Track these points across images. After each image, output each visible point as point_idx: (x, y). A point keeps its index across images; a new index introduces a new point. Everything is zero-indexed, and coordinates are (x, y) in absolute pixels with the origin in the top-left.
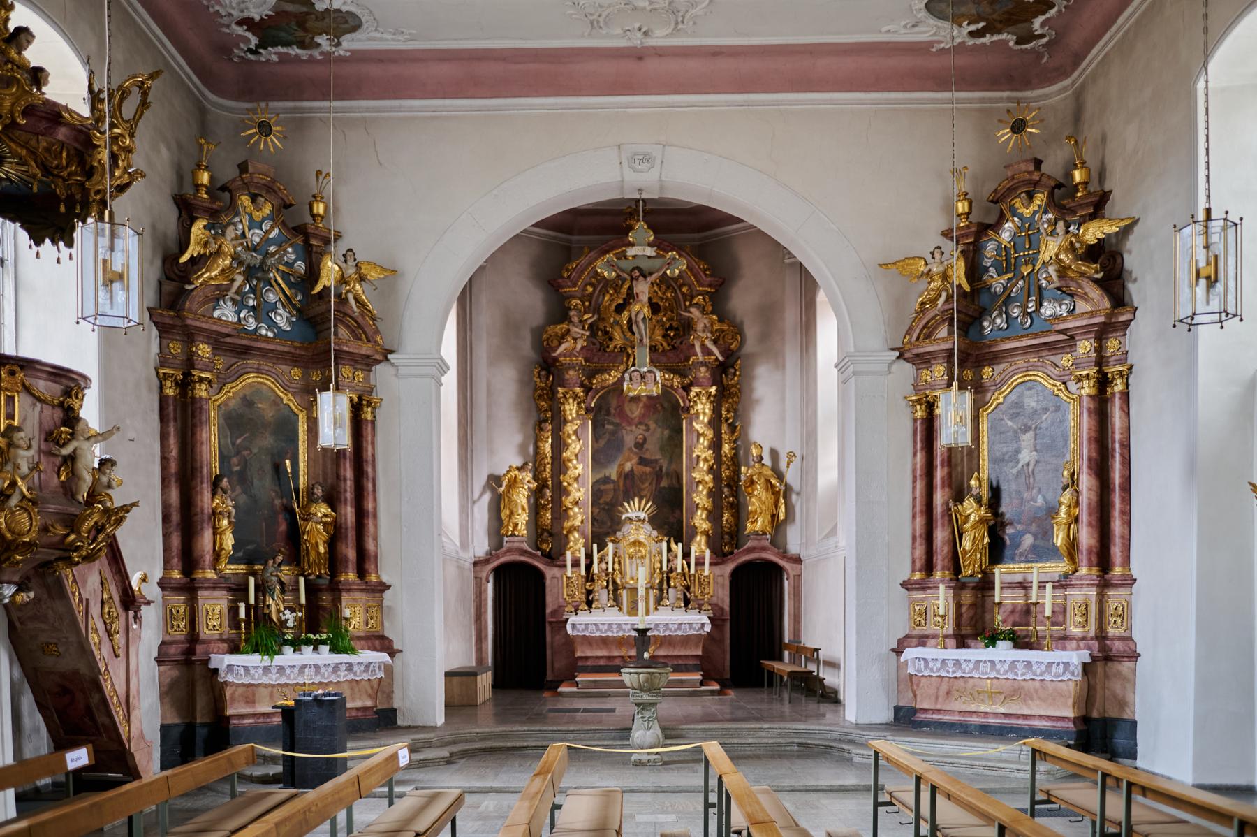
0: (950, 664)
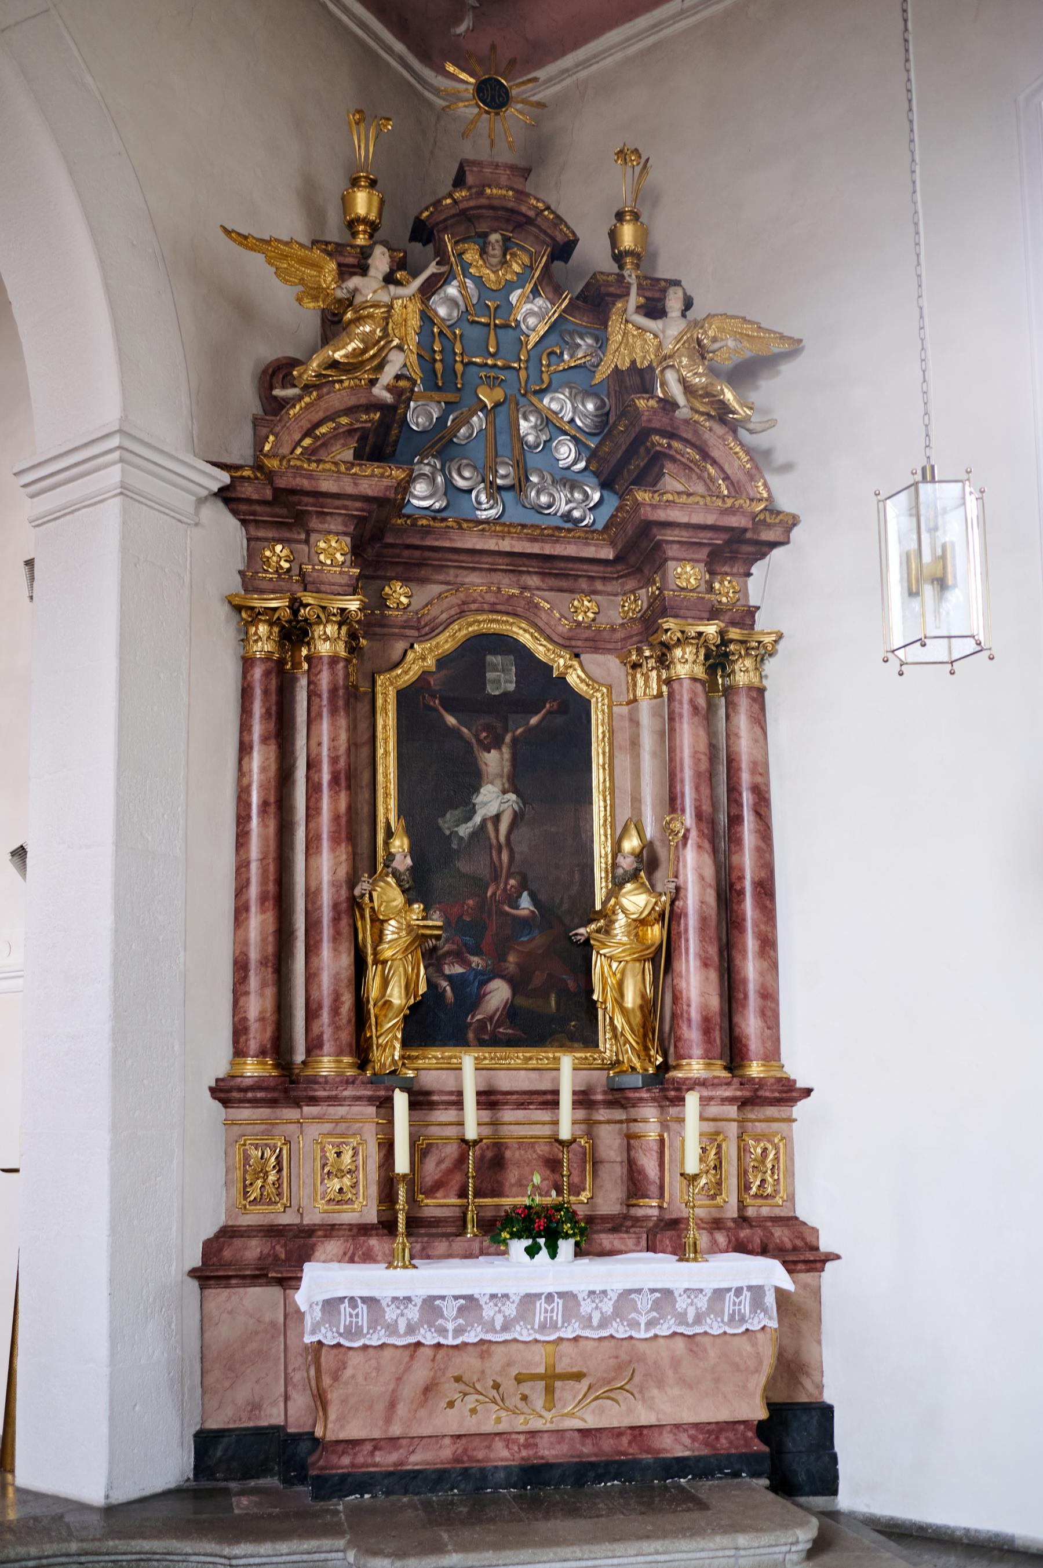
0: (450, 1309)
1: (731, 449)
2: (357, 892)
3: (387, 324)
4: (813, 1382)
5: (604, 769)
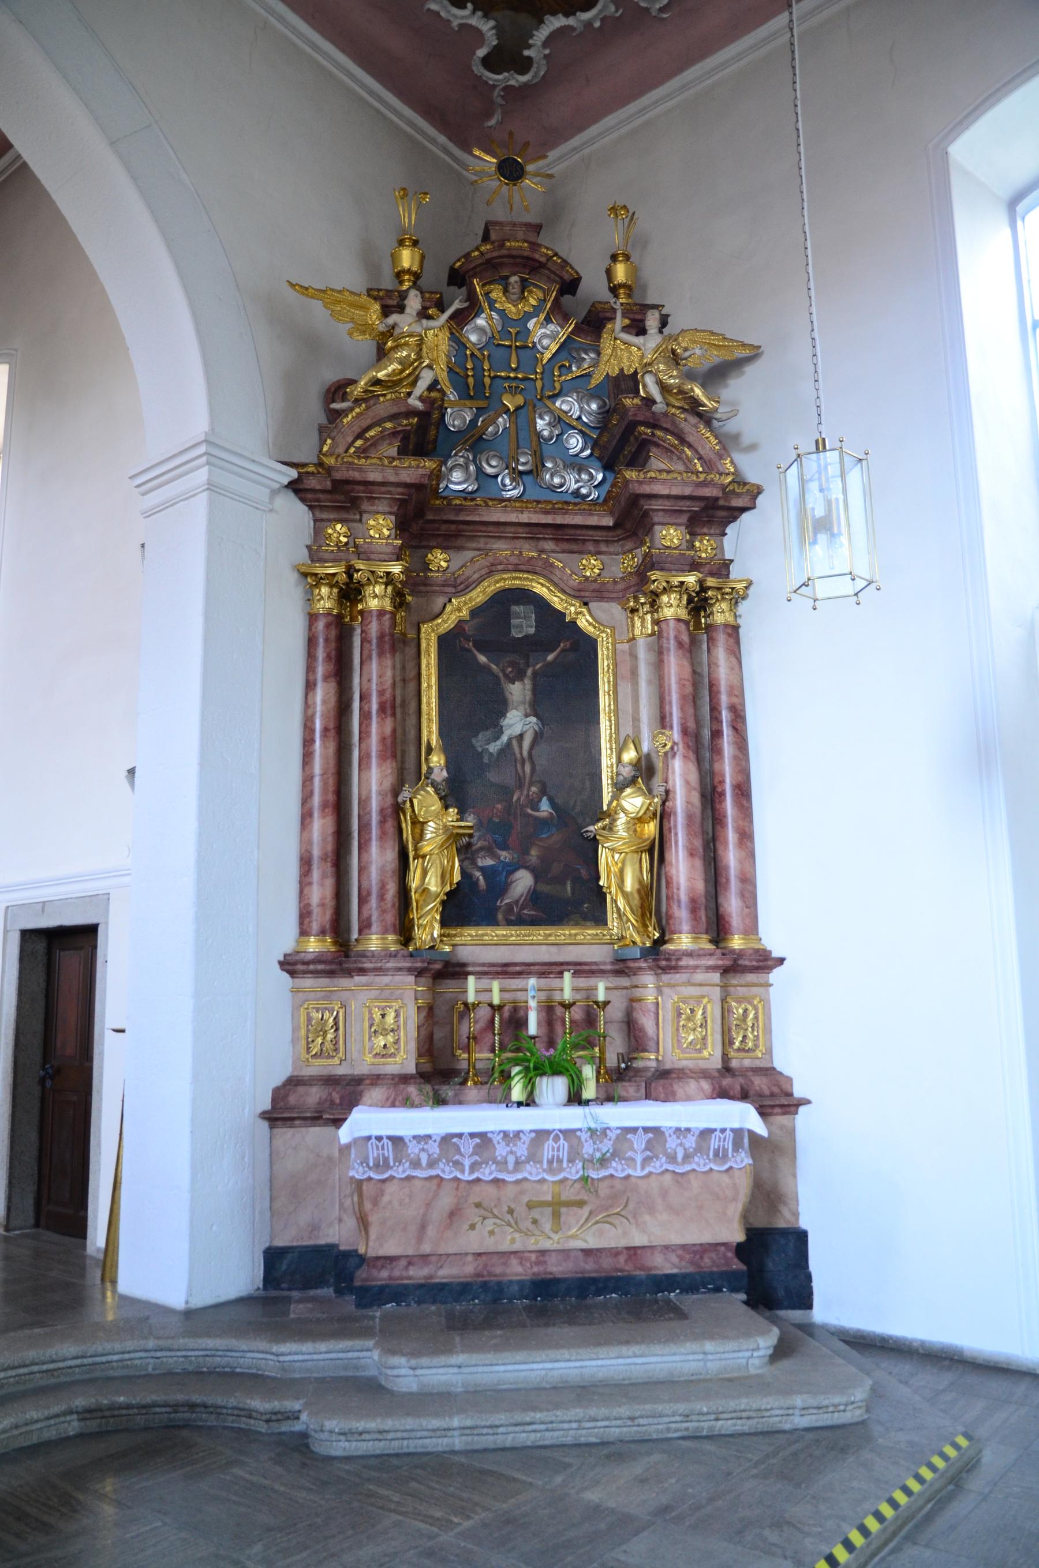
1: (703, 434)
2: (400, 799)
3: (421, 350)
4: (790, 1210)
5: (609, 695)
